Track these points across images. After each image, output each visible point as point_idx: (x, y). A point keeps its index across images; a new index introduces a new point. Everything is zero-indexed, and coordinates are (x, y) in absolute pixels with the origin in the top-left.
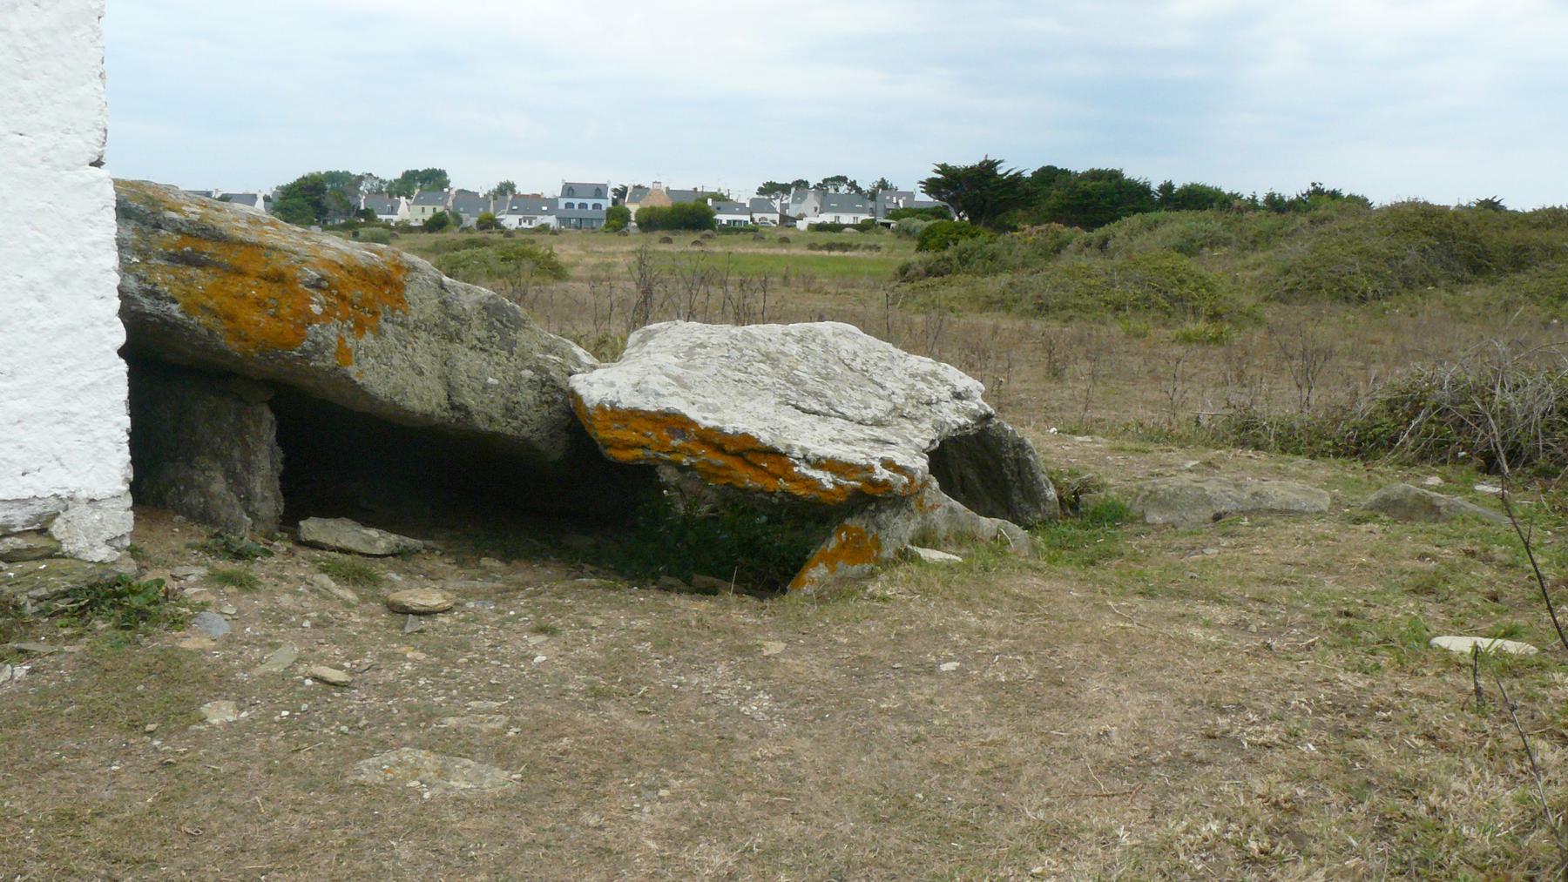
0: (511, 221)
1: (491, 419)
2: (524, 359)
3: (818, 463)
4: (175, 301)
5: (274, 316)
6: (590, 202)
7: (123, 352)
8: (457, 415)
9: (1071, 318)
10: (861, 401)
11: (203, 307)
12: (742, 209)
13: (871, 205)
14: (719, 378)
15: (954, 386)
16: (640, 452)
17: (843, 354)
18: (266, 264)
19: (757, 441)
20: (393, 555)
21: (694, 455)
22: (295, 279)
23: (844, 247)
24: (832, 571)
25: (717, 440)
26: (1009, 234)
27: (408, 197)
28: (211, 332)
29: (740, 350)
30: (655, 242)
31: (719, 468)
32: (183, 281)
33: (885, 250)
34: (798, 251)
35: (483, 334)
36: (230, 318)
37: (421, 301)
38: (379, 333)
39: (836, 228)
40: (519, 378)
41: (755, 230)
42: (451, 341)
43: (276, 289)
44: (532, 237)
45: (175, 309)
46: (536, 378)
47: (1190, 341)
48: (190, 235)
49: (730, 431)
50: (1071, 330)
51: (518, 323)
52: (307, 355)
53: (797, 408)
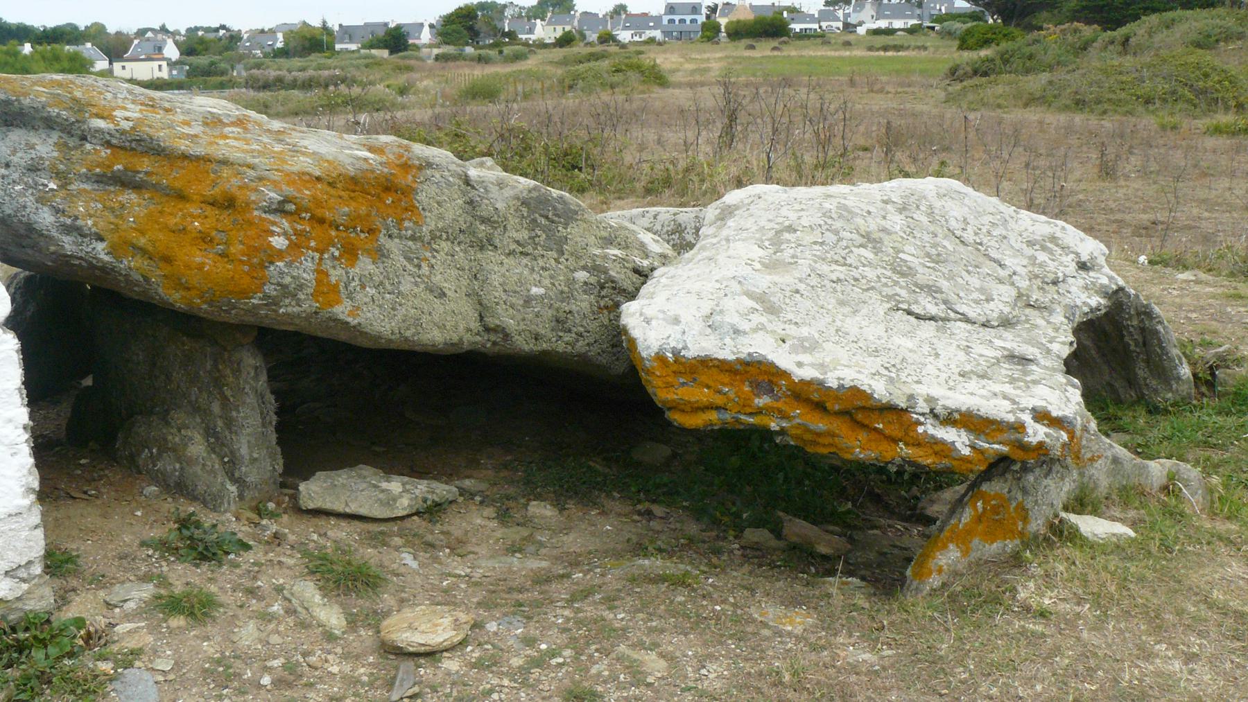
0: (625, 36)
1: (537, 337)
2: (578, 258)
3: (951, 419)
4: (101, 239)
5: (223, 255)
6: (688, 18)
7: (12, 323)
8: (493, 338)
9: (1105, 112)
10: (982, 290)
11: (134, 246)
12: (812, 19)
13: (918, 11)
14: (814, 281)
15: (1077, 254)
16: (713, 416)
17: (953, 224)
18: (214, 184)
19: (869, 397)
20: (417, 513)
21: (784, 416)
22: (248, 204)
23: (897, 48)
24: (966, 553)
25: (815, 397)
26: (1036, 33)
27: (543, 20)
28: (146, 279)
29: (836, 232)
30: (740, 49)
31: (819, 434)
32: (112, 210)
33: (932, 49)
34: (858, 53)
35: (524, 235)
36: (167, 260)
37: (439, 204)
38: (380, 254)
39: (889, 32)
40: (571, 282)
41: (822, 36)
42: (482, 248)
43: (226, 218)
44: (642, 48)
45: (100, 250)
46: (593, 280)
47: (1221, 132)
48: (121, 148)
49: (833, 384)
50: (1108, 124)
51: (570, 216)
52: (273, 302)
53: (909, 313)
